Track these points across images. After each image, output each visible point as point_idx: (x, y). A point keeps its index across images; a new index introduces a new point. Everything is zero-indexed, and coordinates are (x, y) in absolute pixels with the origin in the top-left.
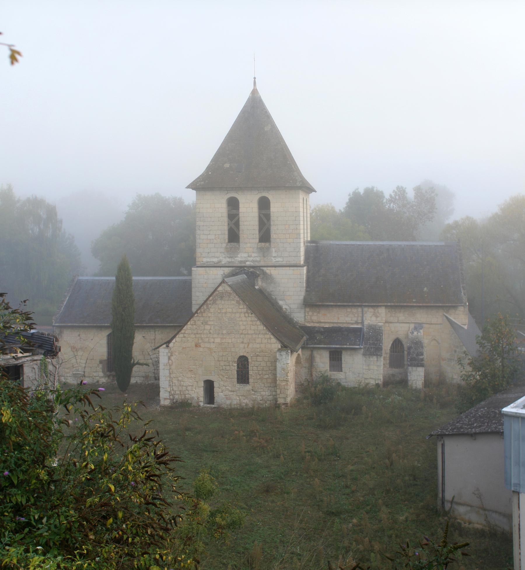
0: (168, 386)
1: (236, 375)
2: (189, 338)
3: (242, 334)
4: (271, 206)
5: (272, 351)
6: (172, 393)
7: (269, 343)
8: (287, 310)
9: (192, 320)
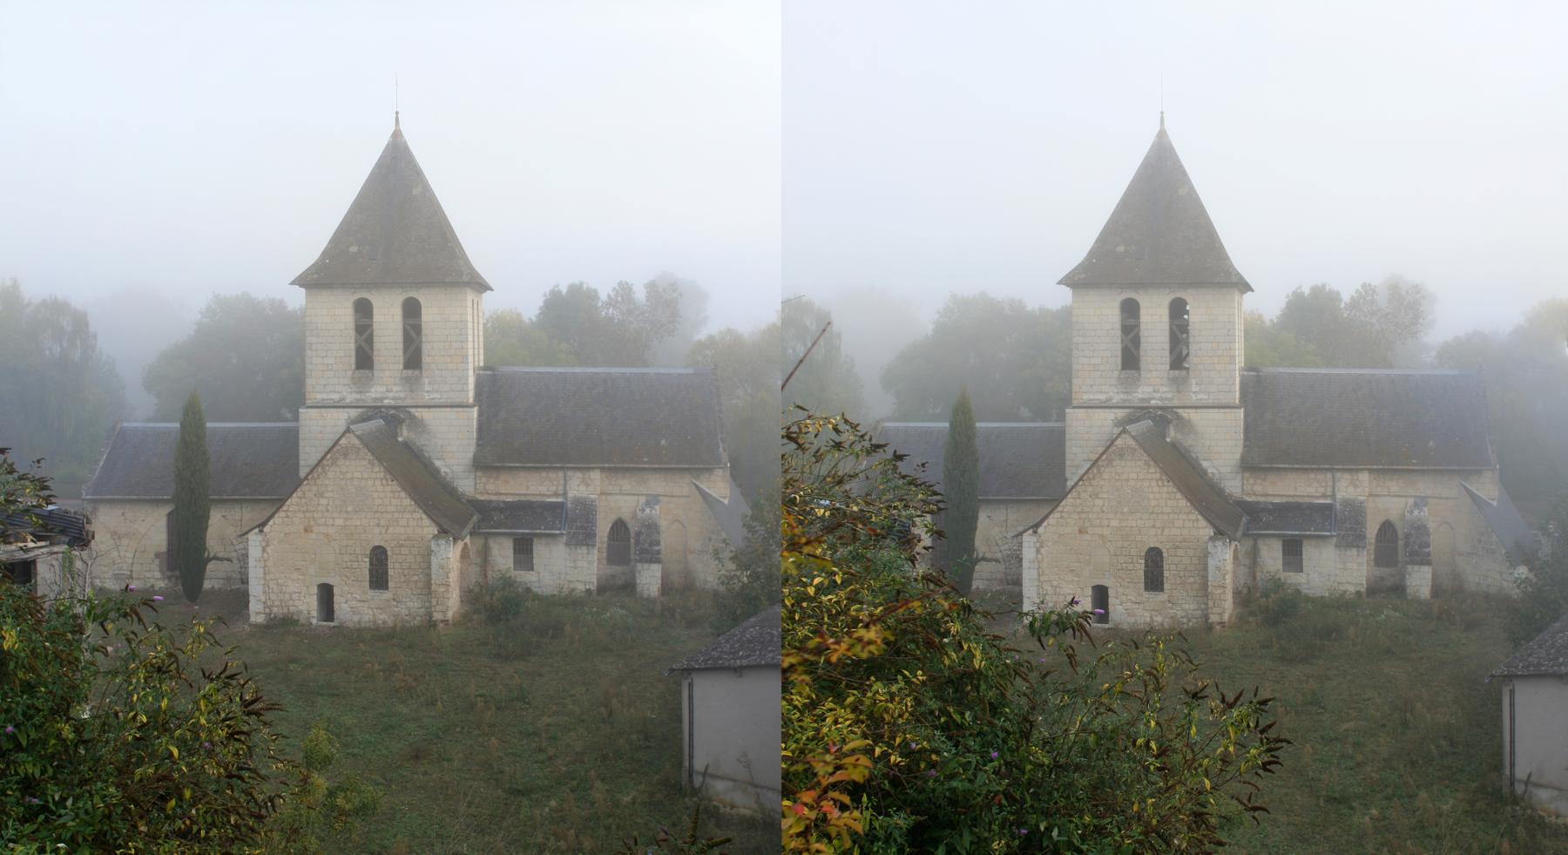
1: (368, 576)
3: (1152, 513)
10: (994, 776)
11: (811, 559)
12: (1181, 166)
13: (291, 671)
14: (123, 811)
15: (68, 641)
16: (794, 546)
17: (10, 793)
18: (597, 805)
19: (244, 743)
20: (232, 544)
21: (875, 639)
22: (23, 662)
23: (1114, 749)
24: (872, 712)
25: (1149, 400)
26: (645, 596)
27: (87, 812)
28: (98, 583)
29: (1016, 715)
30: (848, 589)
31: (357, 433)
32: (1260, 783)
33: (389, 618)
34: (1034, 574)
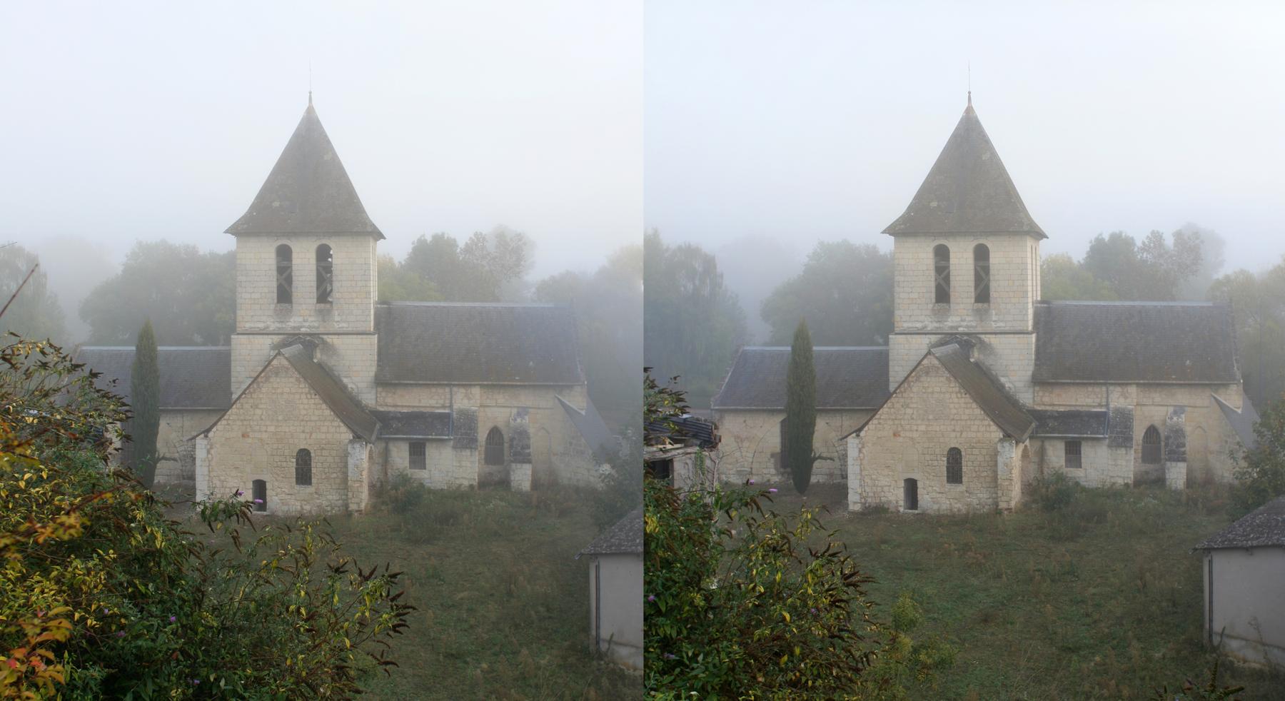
10: (172, 636)
11: (22, 458)
12: (326, 136)
13: (882, 550)
14: (744, 665)
15: (700, 525)
16: (8, 448)
17: (652, 650)
18: (1133, 660)
19: (844, 609)
20: (175, 446)
21: (74, 524)
22: (662, 541)
23: (271, 614)
24: (72, 583)
25: (299, 328)
26: (1173, 488)
27: (715, 666)
28: (724, 478)
29: (190, 586)
30: (53, 483)
31: (937, 355)
32: (391, 642)
33: (963, 506)
34: (205, 470)
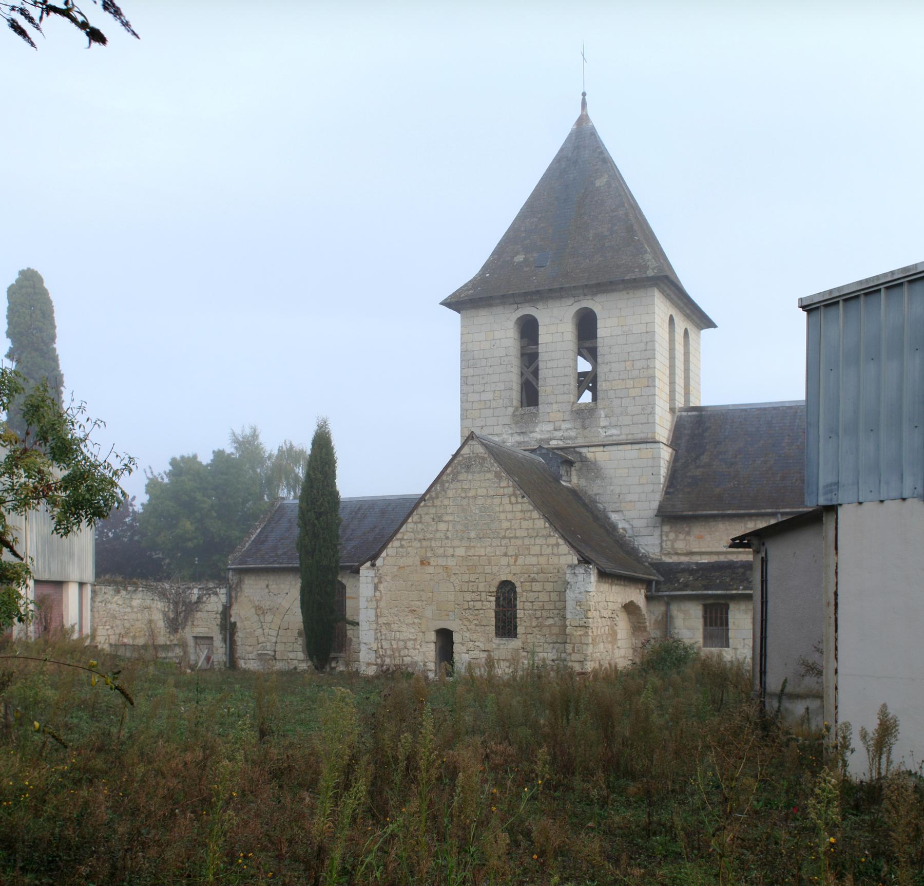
0: (373, 639)
1: (494, 619)
2: (409, 549)
3: (504, 537)
4: (598, 326)
5: (560, 571)
6: (381, 653)
7: (556, 555)
8: (626, 532)
9: (415, 513)
